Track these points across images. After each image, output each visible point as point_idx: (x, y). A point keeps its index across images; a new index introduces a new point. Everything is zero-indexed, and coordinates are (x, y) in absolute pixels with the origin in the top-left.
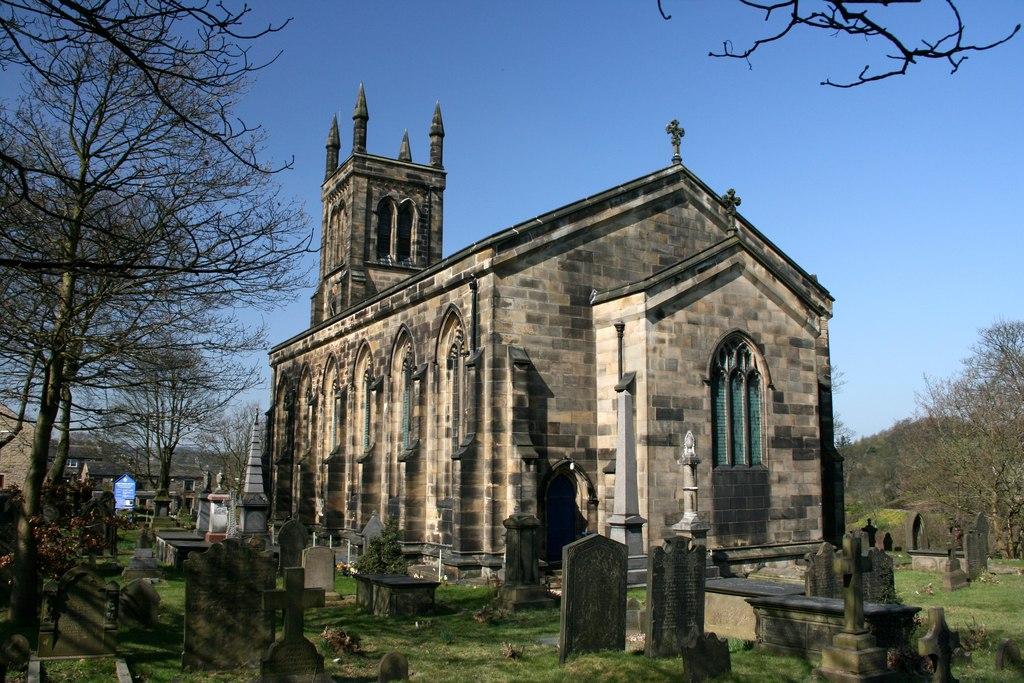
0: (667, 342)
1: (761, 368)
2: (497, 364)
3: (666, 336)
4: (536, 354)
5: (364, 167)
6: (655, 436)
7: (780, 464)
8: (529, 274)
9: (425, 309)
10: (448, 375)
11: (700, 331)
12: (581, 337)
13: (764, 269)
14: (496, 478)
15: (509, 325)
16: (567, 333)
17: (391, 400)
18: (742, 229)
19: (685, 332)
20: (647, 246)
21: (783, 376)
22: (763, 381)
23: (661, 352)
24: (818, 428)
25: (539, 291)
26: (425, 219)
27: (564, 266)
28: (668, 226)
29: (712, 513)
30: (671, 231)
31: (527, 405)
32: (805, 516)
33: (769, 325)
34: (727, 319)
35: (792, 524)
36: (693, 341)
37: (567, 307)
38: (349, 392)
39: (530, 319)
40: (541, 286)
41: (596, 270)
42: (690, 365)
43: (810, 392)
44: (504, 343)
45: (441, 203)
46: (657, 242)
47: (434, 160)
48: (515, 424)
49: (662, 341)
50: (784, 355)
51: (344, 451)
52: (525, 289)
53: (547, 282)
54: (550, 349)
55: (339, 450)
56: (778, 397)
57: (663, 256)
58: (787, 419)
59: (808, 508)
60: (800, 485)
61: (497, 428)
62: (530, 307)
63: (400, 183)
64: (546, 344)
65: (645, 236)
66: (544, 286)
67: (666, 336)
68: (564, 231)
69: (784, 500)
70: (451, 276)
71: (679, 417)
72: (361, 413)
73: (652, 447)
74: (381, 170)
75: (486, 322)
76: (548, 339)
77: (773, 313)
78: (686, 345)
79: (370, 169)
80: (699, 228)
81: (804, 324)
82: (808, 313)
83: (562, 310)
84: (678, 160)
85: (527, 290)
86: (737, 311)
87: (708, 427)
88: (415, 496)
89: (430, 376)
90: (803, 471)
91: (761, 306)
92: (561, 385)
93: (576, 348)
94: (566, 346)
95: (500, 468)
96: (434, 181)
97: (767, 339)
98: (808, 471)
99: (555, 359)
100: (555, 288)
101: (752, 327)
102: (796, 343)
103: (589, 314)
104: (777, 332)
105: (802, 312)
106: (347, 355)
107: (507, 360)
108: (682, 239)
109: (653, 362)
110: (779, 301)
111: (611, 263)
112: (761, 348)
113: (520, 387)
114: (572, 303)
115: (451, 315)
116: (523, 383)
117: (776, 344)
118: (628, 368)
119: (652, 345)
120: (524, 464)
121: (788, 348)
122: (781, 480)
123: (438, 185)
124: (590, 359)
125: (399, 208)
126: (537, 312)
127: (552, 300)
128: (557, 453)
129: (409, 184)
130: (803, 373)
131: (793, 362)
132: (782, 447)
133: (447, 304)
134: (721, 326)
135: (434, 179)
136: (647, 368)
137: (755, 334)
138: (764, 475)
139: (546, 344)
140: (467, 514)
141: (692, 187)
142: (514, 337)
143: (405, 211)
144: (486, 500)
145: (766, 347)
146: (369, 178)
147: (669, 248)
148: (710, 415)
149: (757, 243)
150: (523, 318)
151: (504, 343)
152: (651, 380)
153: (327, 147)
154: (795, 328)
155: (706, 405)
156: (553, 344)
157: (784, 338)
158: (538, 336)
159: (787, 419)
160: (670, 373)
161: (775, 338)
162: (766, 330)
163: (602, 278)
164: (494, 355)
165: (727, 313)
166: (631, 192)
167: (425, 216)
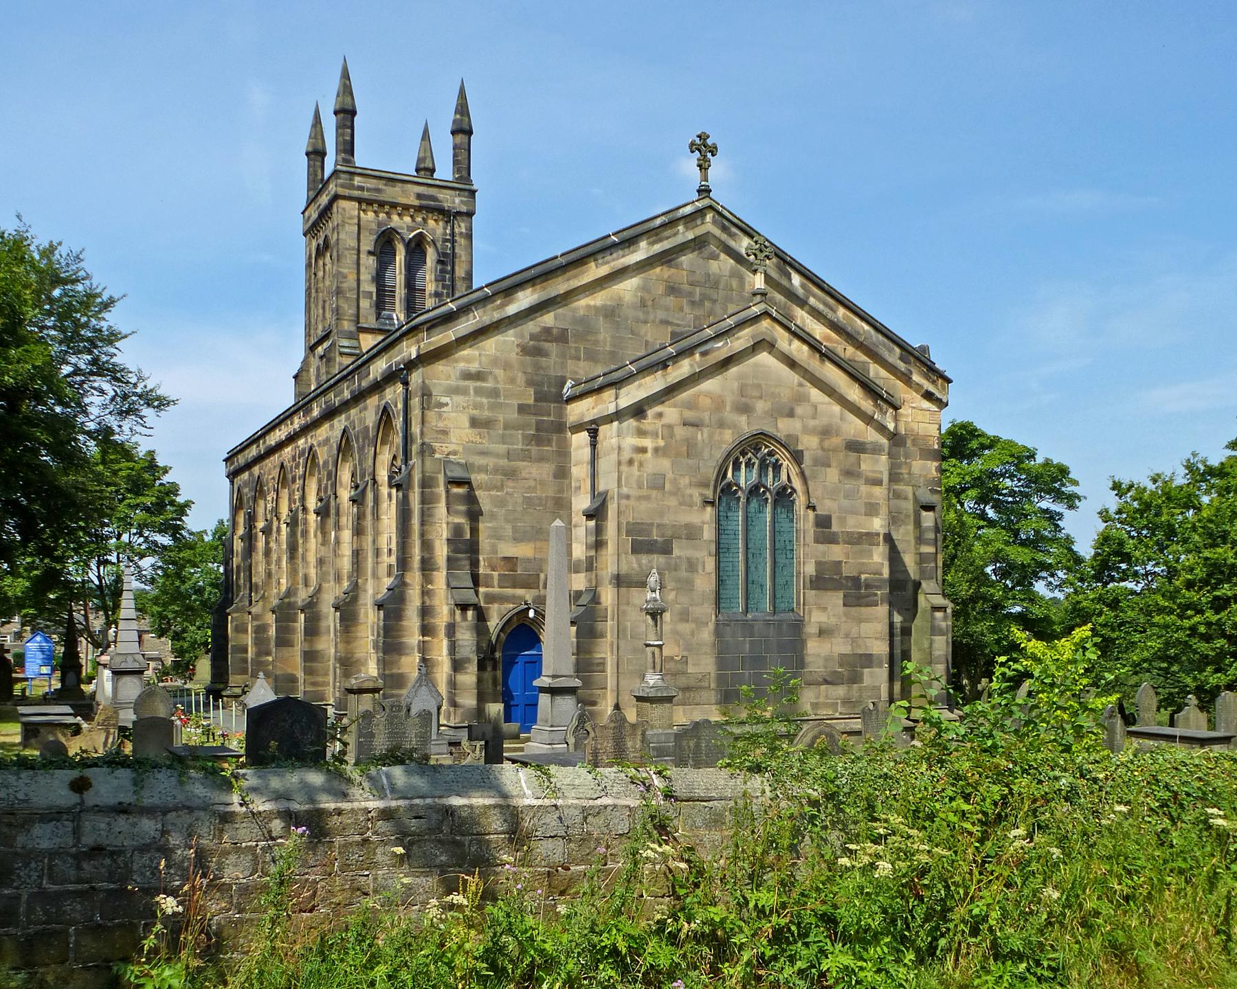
0: (650, 451)
1: (797, 483)
2: (426, 483)
3: (648, 443)
4: (483, 469)
5: (352, 187)
6: (627, 575)
7: (822, 611)
8: (470, 358)
9: (365, 408)
10: (390, 495)
11: (701, 436)
12: (549, 444)
13: (805, 348)
14: (426, 630)
15: (445, 432)
16: (529, 440)
17: (338, 527)
18: (803, 286)
19: (678, 438)
20: (651, 317)
21: (833, 494)
22: (800, 500)
23: (641, 464)
24: (886, 564)
25: (489, 384)
26: (446, 260)
27: (525, 350)
28: (686, 287)
29: (713, 675)
30: (691, 294)
31: (468, 537)
32: (861, 681)
33: (812, 423)
34: (744, 418)
35: (840, 691)
36: (691, 449)
37: (529, 406)
38: (300, 515)
39: (474, 423)
40: (490, 379)
41: (573, 351)
42: (685, 481)
43: (877, 515)
44: (437, 456)
45: (469, 236)
46: (667, 309)
47: (459, 171)
48: (449, 560)
49: (643, 450)
50: (834, 464)
51: (295, 594)
52: (467, 383)
53: (499, 373)
54: (503, 462)
55: (290, 592)
56: (823, 522)
57: (678, 329)
58: (836, 552)
59: (866, 671)
60: (854, 640)
61: (427, 566)
62: (475, 407)
63: (406, 207)
64: (498, 456)
65: (650, 303)
66: (496, 378)
67: (648, 443)
68: (525, 299)
69: (827, 659)
70: (384, 366)
71: (666, 549)
72: (313, 543)
73: (623, 590)
74: (378, 190)
75: (416, 429)
76: (502, 448)
77: (820, 408)
78: (678, 455)
79: (361, 188)
80: (734, 286)
81: (868, 419)
82: (876, 405)
83: (522, 409)
84: (704, 191)
85: (472, 384)
86: (761, 406)
87: (710, 564)
88: (353, 653)
89: (370, 495)
90: (860, 621)
91: (801, 398)
92: (520, 509)
93: (541, 459)
94: (526, 456)
95: (433, 617)
96: (453, 201)
97: (809, 443)
98: (867, 620)
99: (511, 474)
100: (512, 381)
101: (784, 428)
102: (856, 447)
103: (561, 414)
104: (825, 432)
105: (867, 405)
106: (297, 466)
107: (441, 479)
108: (707, 304)
109: (627, 478)
110: (830, 391)
111: (596, 342)
112: (797, 457)
113: (457, 513)
114: (536, 400)
115: (386, 415)
116: (463, 508)
117: (823, 449)
118: (601, 487)
119: (626, 455)
120: (458, 612)
121: (841, 455)
122: (823, 632)
123: (464, 209)
124: (562, 473)
125: (408, 245)
126: (486, 414)
127: (506, 397)
128: (514, 597)
129: (419, 209)
130: (864, 489)
131: (850, 473)
132: (826, 589)
133: (383, 402)
134: (734, 426)
135: (457, 200)
136: (619, 486)
137: (788, 436)
138: (797, 626)
139: (498, 456)
140: (392, 676)
141: (724, 229)
142: (452, 447)
143: (416, 248)
144: (417, 657)
145: (805, 453)
146: (360, 203)
147: (686, 318)
148: (713, 548)
149: (826, 304)
150: (465, 421)
151: (437, 456)
152: (624, 502)
153: (307, 154)
154: (854, 427)
155: (708, 533)
156: (509, 455)
157: (836, 441)
158: (486, 445)
159: (836, 552)
160: (654, 493)
161: (822, 441)
162: (806, 430)
163: (582, 364)
164: (423, 472)
165: (745, 409)
166: (628, 241)
167: (445, 255)
